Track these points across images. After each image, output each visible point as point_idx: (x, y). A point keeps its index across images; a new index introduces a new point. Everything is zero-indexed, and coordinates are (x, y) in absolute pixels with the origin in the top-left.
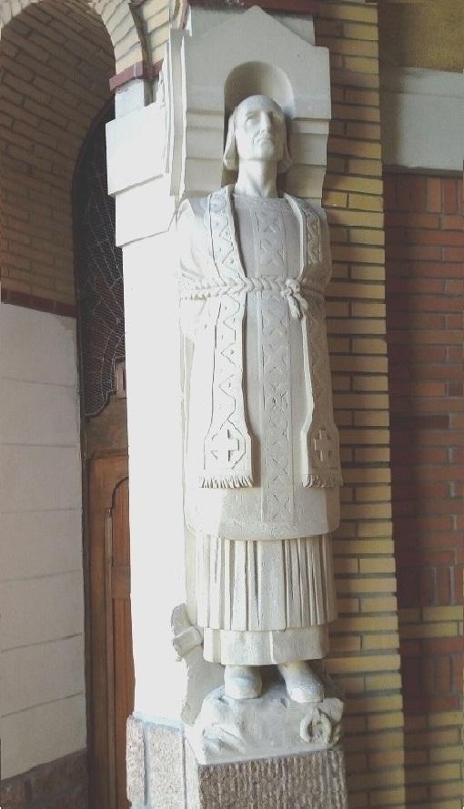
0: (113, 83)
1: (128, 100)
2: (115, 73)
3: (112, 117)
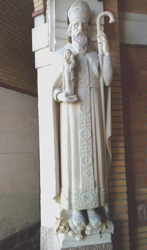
1: (39, 21)
2: (34, 12)
3: (34, 27)
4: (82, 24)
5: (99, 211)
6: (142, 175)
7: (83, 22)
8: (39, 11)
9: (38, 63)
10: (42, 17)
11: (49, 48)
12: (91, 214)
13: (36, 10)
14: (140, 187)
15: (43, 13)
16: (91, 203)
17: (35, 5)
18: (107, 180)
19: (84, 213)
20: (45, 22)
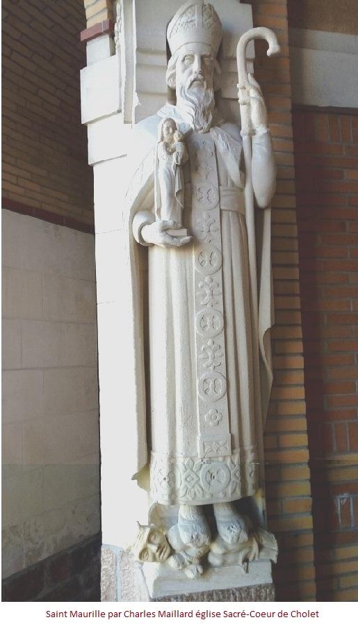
0: (84, 36)
1: (97, 50)
2: (86, 28)
3: (85, 65)
4: (202, 58)
5: (242, 507)
6: (346, 421)
7: (204, 53)
8: (98, 25)
9: (95, 153)
10: (106, 40)
11: (121, 116)
12: (223, 515)
13: (90, 24)
14: (342, 451)
15: (106, 32)
16: (223, 489)
17: (89, 13)
18: (261, 433)
19: (206, 513)
20: (113, 53)
